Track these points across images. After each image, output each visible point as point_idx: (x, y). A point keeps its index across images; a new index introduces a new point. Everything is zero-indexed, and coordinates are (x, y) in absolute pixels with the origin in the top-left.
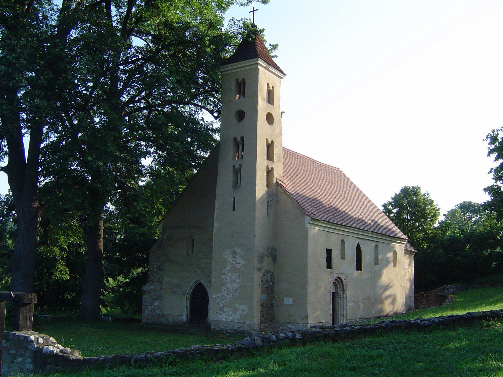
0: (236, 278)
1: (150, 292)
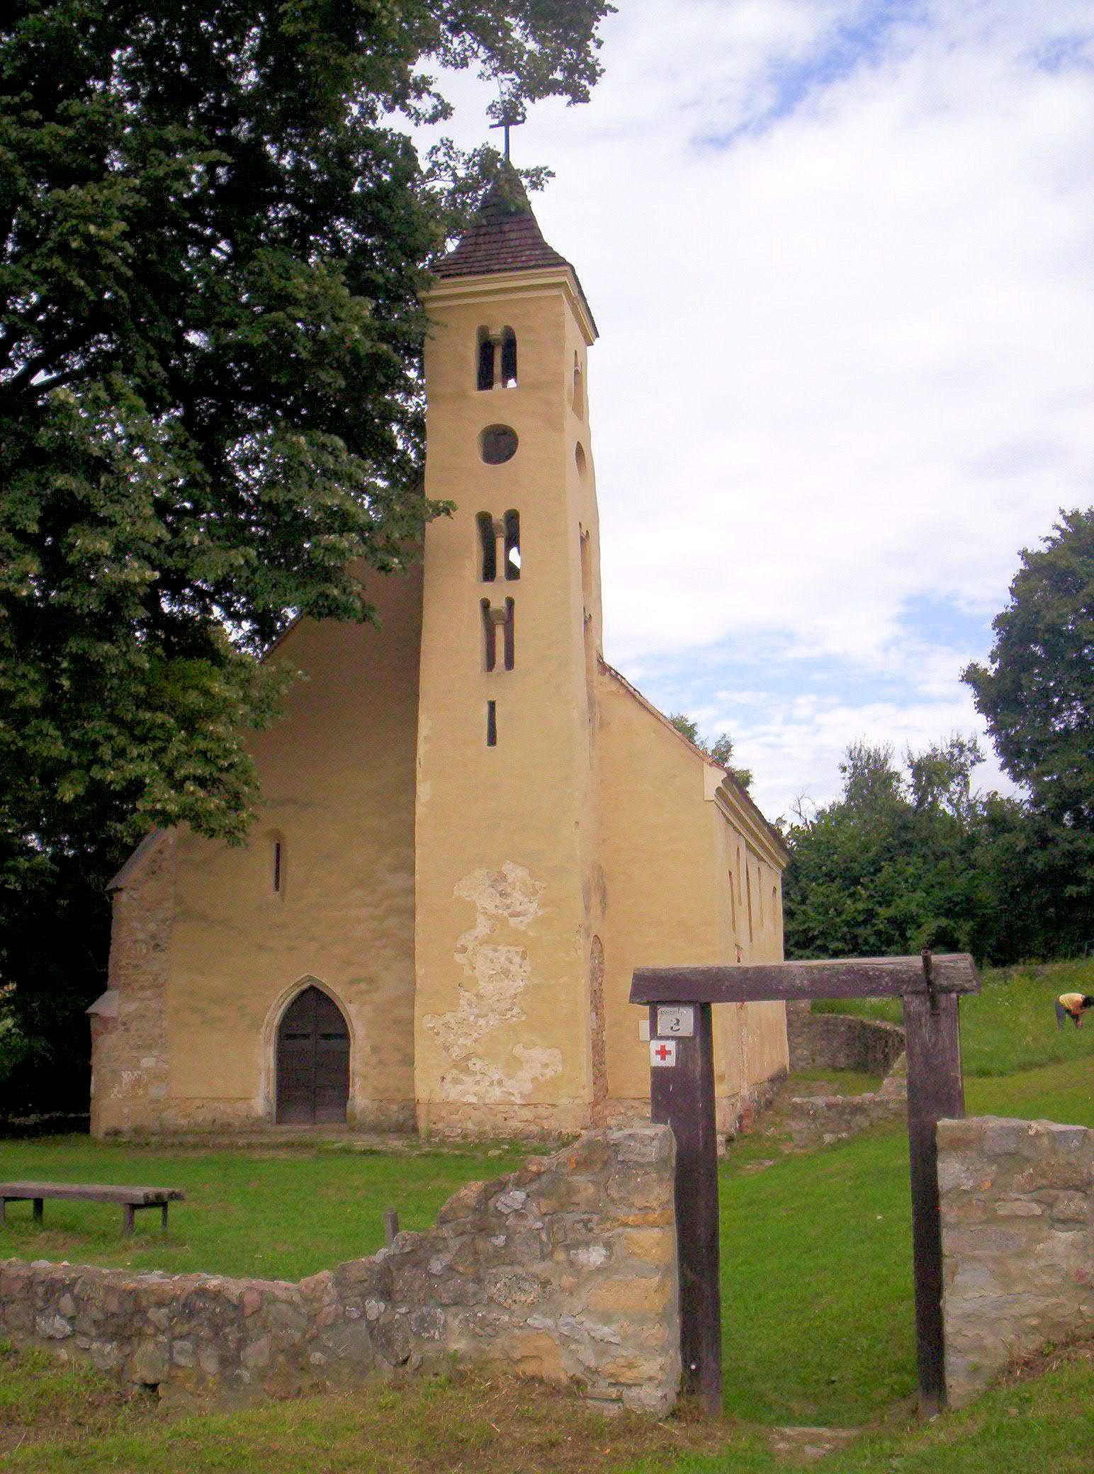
0: (511, 963)
1: (124, 1024)
